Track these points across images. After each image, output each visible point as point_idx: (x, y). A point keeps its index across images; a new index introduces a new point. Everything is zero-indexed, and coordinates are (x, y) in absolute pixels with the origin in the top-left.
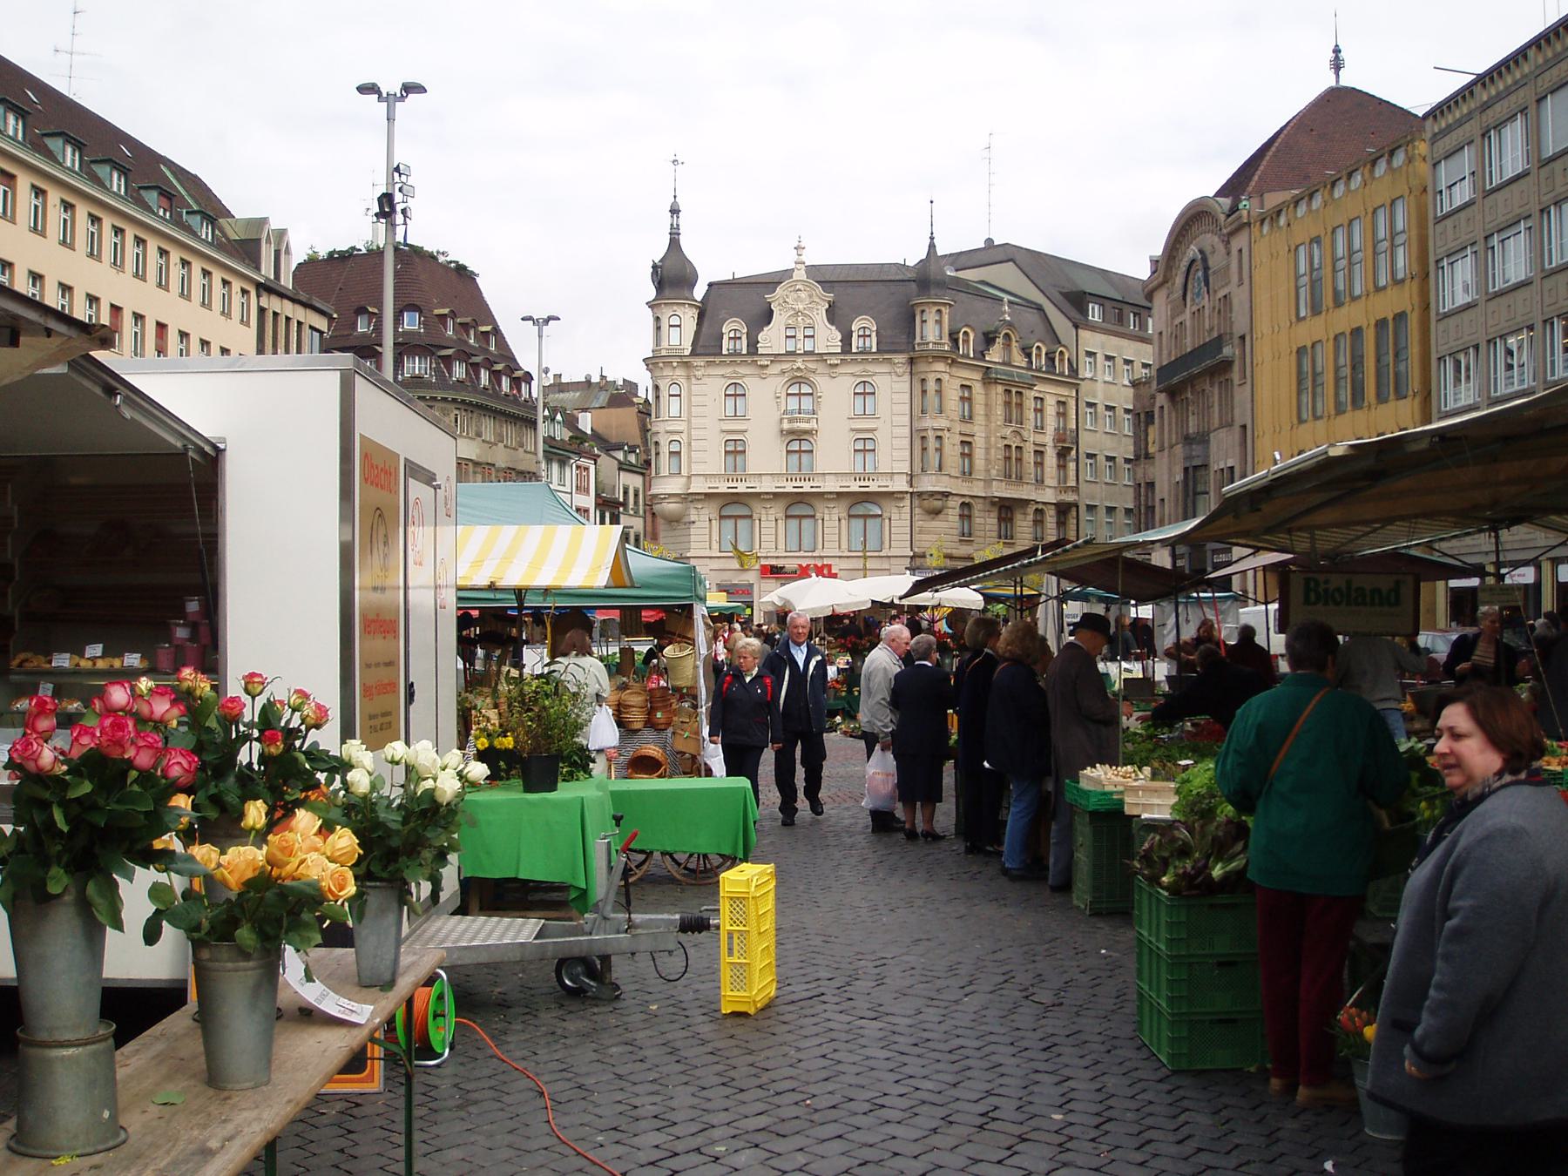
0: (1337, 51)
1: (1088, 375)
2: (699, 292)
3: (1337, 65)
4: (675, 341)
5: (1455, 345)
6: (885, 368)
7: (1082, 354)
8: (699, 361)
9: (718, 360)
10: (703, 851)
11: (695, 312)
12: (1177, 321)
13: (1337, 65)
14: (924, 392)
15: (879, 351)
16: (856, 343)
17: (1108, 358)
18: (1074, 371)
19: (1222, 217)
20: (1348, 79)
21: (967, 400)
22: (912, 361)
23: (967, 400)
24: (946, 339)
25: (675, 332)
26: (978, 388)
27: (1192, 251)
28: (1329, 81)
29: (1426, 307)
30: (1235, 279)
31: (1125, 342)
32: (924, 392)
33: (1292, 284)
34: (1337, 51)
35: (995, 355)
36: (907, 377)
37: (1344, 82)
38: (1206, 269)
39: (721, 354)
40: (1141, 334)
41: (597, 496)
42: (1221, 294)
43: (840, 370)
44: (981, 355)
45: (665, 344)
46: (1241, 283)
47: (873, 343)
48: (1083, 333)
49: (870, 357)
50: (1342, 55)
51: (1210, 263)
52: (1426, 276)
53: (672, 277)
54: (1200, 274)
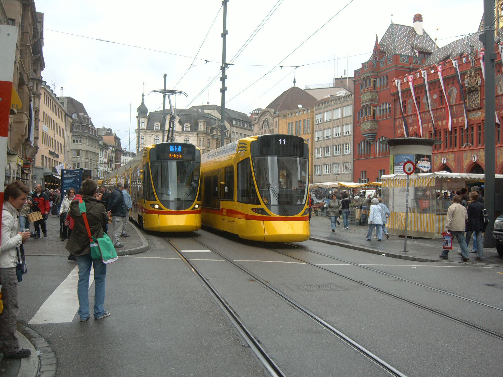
0: (295, 79)
1: (233, 137)
2: (148, 114)
3: (295, 82)
4: (143, 126)
5: (317, 146)
6: (192, 135)
7: (232, 132)
8: (149, 131)
9: (153, 131)
10: (365, 170)
11: (147, 120)
12: (260, 131)
13: (295, 82)
14: (200, 141)
15: (190, 131)
16: (185, 128)
17: (237, 133)
18: (230, 136)
19: (273, 114)
20: (297, 85)
21: (209, 143)
22: (198, 134)
23: (209, 143)
24: (205, 129)
25: (143, 124)
26: (211, 140)
27: (265, 118)
28: (292, 85)
29: (313, 139)
30: (275, 126)
31: (240, 129)
32: (200, 141)
33: (287, 130)
34: (295, 79)
35: (214, 133)
36: (196, 137)
37: (296, 86)
38: (268, 123)
39: (154, 130)
40: (240, 126)
41: (108, 159)
42: (271, 128)
43: (182, 135)
44: (211, 133)
45: (140, 127)
46: (276, 127)
47: (189, 129)
48: (232, 128)
49: (188, 132)
50: (296, 80)
51: (269, 122)
52: (313, 133)
53: (142, 110)
54: (266, 123)
